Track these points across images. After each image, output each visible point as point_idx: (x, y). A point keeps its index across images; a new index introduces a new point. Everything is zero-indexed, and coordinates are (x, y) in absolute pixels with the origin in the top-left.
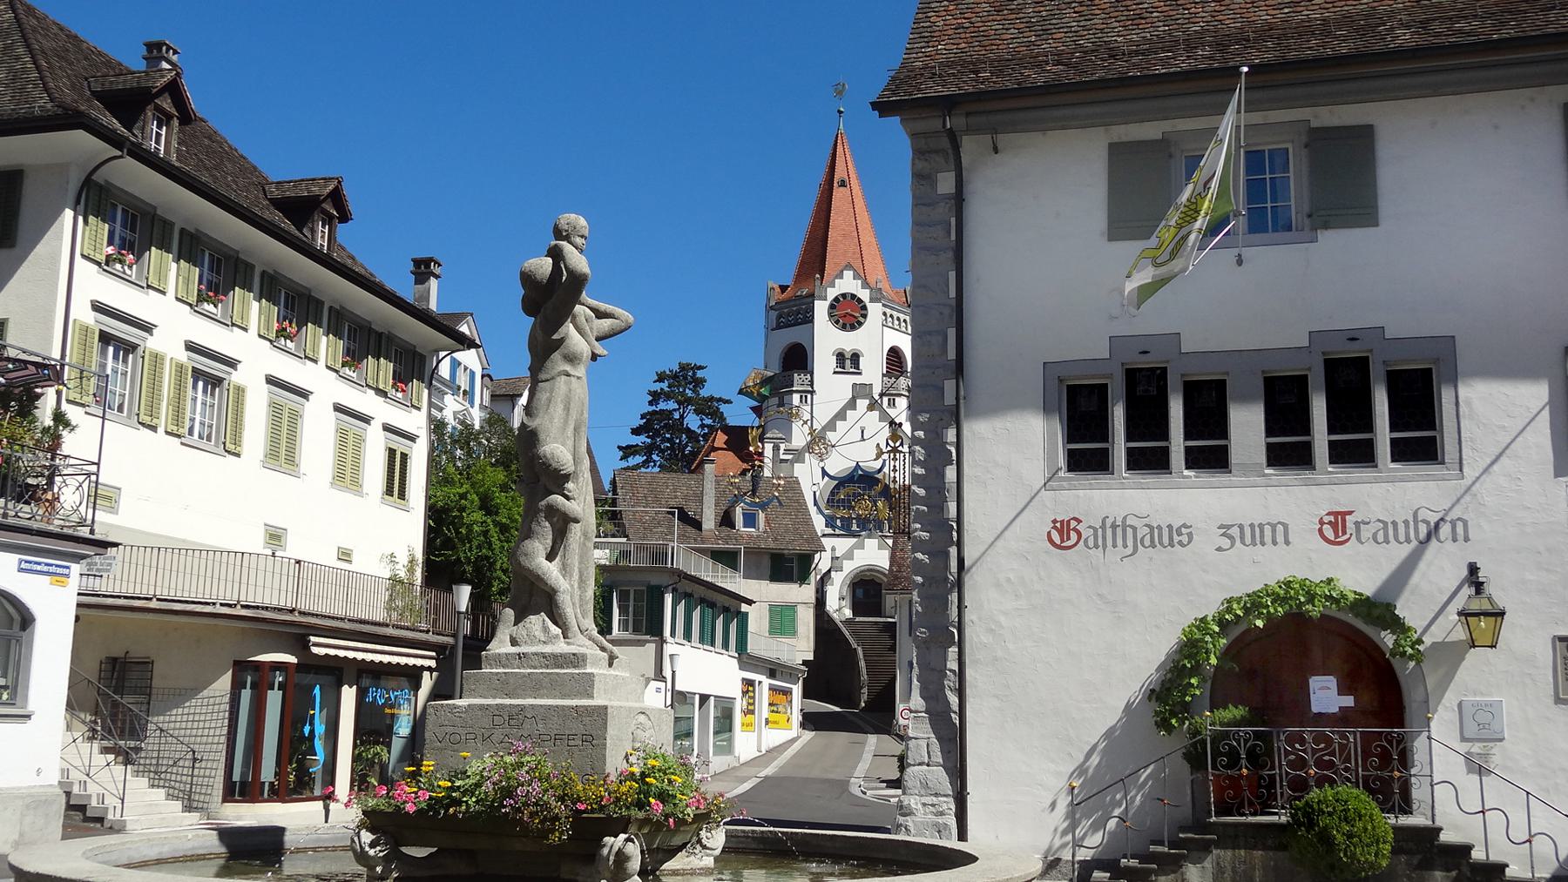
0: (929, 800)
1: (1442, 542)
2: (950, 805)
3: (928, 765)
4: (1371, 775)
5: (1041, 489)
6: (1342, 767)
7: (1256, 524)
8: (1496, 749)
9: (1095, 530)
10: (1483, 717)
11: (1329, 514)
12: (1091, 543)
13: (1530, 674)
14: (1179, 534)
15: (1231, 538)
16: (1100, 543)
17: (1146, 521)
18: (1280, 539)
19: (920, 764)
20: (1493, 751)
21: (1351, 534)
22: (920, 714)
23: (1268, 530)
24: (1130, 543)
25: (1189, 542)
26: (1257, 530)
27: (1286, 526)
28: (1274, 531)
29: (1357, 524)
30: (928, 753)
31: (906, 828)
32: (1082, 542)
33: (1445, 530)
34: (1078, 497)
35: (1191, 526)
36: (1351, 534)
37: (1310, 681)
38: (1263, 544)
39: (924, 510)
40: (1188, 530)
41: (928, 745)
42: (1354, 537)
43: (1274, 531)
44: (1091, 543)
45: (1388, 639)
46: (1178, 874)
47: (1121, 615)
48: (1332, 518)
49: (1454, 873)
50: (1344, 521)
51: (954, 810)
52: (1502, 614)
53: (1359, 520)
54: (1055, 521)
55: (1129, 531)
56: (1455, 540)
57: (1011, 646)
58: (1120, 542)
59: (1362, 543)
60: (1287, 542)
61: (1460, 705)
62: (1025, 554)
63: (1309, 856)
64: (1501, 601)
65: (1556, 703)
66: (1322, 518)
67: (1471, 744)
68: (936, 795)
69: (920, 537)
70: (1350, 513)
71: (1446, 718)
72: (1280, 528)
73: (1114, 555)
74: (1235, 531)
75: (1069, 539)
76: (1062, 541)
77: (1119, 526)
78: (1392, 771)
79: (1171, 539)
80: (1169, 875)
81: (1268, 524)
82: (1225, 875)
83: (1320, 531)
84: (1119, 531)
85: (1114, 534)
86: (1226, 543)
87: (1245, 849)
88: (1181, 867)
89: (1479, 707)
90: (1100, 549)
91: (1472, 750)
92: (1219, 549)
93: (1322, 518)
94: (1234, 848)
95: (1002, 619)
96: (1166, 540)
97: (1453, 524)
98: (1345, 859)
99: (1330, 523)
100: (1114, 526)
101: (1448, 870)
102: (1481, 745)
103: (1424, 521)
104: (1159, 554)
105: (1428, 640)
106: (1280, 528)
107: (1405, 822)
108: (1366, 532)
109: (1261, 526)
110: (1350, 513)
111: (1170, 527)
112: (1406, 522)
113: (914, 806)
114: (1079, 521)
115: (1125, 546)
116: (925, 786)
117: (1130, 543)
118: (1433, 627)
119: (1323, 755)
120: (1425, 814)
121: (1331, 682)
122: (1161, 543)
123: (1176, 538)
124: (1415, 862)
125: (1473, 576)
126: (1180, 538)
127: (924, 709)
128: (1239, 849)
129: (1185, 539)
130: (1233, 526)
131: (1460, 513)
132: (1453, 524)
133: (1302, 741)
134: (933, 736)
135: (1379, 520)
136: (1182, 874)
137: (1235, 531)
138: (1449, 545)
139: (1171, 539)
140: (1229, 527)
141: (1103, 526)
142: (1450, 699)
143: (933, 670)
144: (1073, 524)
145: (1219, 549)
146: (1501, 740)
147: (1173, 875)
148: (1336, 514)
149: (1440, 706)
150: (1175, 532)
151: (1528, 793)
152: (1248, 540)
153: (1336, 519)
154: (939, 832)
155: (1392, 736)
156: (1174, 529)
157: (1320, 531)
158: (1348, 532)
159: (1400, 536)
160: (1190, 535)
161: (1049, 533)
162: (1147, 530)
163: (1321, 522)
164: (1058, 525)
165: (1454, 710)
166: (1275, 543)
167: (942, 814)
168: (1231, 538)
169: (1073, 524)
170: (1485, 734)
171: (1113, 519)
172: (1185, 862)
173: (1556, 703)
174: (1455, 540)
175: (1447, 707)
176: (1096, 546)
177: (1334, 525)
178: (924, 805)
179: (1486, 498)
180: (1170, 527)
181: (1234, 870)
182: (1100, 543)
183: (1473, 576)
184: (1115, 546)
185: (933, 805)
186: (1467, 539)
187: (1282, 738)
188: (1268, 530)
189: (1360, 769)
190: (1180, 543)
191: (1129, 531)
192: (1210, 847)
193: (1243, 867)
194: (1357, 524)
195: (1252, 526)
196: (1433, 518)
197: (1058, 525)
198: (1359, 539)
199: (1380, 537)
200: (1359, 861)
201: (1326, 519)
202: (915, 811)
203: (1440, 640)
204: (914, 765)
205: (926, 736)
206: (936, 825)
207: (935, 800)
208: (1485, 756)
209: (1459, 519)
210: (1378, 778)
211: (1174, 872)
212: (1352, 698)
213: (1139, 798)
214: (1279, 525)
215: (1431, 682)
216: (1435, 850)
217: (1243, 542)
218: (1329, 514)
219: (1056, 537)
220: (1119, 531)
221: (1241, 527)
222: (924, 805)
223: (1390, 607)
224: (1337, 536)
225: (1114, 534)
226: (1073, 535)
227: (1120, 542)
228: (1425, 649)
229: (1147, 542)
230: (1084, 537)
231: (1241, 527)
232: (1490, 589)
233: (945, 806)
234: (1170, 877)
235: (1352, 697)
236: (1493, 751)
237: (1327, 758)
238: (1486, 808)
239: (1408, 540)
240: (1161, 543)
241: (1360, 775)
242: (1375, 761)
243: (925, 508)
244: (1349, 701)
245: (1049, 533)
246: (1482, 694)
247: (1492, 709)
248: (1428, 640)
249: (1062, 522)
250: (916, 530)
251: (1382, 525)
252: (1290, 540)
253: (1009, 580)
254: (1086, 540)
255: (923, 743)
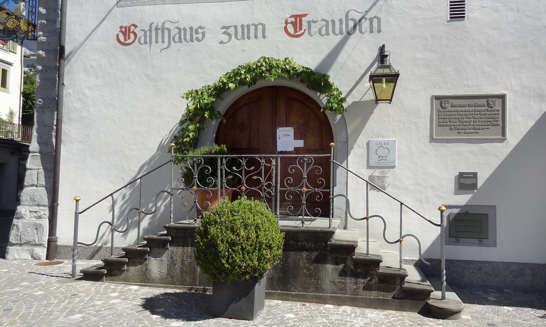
0: (34, 208)
1: (363, 34)
2: (46, 212)
3: (37, 186)
4: (286, 191)
5: (114, 7)
6: (266, 184)
7: (245, 25)
8: (389, 174)
9: (145, 32)
10: (382, 152)
11: (291, 17)
12: (142, 41)
13: (415, 122)
14: (197, 33)
15: (229, 35)
16: (148, 40)
17: (176, 25)
18: (260, 34)
19: (32, 186)
20: (387, 175)
21: (305, 30)
22: (36, 154)
23: (252, 29)
24: (166, 40)
25: (203, 38)
26: (246, 29)
27: (264, 26)
28: (256, 29)
29: (309, 23)
30: (37, 178)
31: (17, 227)
32: (137, 41)
33: (365, 24)
34: (136, 10)
35: (204, 28)
36: (305, 30)
37: (278, 130)
38: (249, 38)
39: (44, 23)
40: (202, 30)
41: (38, 174)
42: (306, 32)
43: (256, 29)
44: (142, 41)
45: (323, 99)
46: (143, 266)
47: (159, 88)
48: (293, 19)
49: (341, 266)
50: (301, 21)
51: (48, 215)
52: (397, 76)
53: (311, 20)
54: (121, 27)
55: (166, 32)
56: (371, 32)
57: (92, 110)
58: (160, 39)
59: (312, 36)
60: (264, 37)
61: (368, 144)
62: (103, 49)
63: (61, 296)
64: (396, 68)
65: (431, 142)
66: (287, 20)
67: (374, 170)
68: (39, 205)
69: (41, 40)
70: (305, 15)
71: (358, 153)
72: (260, 27)
73: (156, 48)
74: (232, 31)
75: (129, 38)
76: (125, 40)
77: (160, 29)
78: (301, 187)
79: (191, 36)
80: (137, 266)
81: (253, 24)
82: (176, 266)
83: (286, 28)
84: (160, 32)
85: (157, 35)
86: (225, 38)
87: (192, 246)
88: (146, 259)
89: (381, 145)
90: (148, 44)
91: (374, 174)
92: (221, 43)
93: (287, 20)
94: (183, 246)
95: (87, 92)
96: (188, 37)
97: (371, 20)
98: (227, 266)
99: (292, 23)
100: (157, 29)
101: (337, 264)
102: (380, 170)
103: (353, 19)
104: (183, 47)
105: (349, 101)
106: (260, 27)
107: (311, 225)
108: (315, 28)
109: (248, 26)
110: (305, 15)
111: (191, 28)
112: (341, 21)
113: (23, 213)
114: (136, 26)
115: (163, 42)
116: (33, 200)
117: (166, 40)
118: (354, 92)
119: (253, 175)
120: (341, 217)
121: (290, 131)
122: (185, 39)
123: (195, 36)
124: (313, 257)
125: (382, 56)
126: (197, 36)
127: (38, 151)
128: (187, 246)
129: (200, 36)
130: (230, 27)
131: (376, 13)
132: (371, 20)
133: (239, 165)
134: (41, 167)
135: (323, 20)
136: (146, 265)
137: (232, 31)
138: (368, 35)
139: (191, 36)
140: (228, 28)
141: (150, 30)
142: (362, 140)
143: (46, 125)
144: (132, 28)
145: (221, 43)
146: (393, 167)
147: (140, 266)
148: (296, 16)
149: (355, 145)
150: (194, 32)
151: (402, 204)
152: (240, 36)
153: (296, 20)
154: (37, 229)
155: (303, 160)
156: (194, 30)
157: (286, 28)
158: (303, 28)
159: (336, 30)
160: (204, 34)
161: (118, 35)
162: (177, 31)
163: (286, 22)
164: (123, 30)
165: (364, 147)
166: (256, 37)
167: (40, 217)
168: (229, 35)
169: (132, 28)
170: (383, 163)
171: (157, 25)
172: (149, 256)
173: (431, 142)
174: (371, 32)
175: (359, 145)
176: (146, 43)
177: (294, 24)
178: (31, 212)
179: (393, 2)
180: (191, 28)
181: (183, 263)
182: (148, 40)
183: (382, 56)
184: (157, 42)
185: (35, 212)
186: (379, 31)
187: (224, 161)
188: (252, 29)
189: (279, 186)
190: (197, 39)
191: (166, 32)
192: (166, 244)
193: (189, 260)
194: (309, 23)
195: (243, 26)
196: (358, 17)
197: (123, 30)
198: (310, 33)
199: (323, 31)
200: (240, 267)
201: (290, 20)
202: (24, 216)
203: (358, 100)
204: (28, 186)
205: (37, 167)
206: (35, 224)
207: (37, 208)
208: (382, 178)
209: (375, 17)
210: (290, 193)
211: (141, 263)
212: (302, 141)
213: (162, 207)
214: (259, 25)
215: (350, 129)
216: (329, 249)
217: (236, 37)
218: (291, 17)
219: (291, 29)
220: (160, 32)
221: (236, 27)
222: (31, 212)
223: (325, 77)
224: (296, 31)
225: (157, 35)
226: (132, 36)
227: (160, 39)
228: (348, 106)
229: (177, 39)
230: (138, 37)
231: (236, 27)
232: (390, 60)
233: (42, 213)
234: (137, 267)
235: (303, 140)
236: (387, 175)
237: (255, 177)
238: (369, 215)
239: (341, 33)
240: (185, 39)
241: (278, 190)
242: (206, 172)
243: (45, 21)
244: (300, 143)
245: (118, 35)
246: (383, 136)
247: (388, 146)
248: (349, 101)
249: (126, 28)
250: (40, 35)
251: (325, 23)
252: (266, 35)
253: (92, 66)
254: (140, 39)
255: (35, 172)
